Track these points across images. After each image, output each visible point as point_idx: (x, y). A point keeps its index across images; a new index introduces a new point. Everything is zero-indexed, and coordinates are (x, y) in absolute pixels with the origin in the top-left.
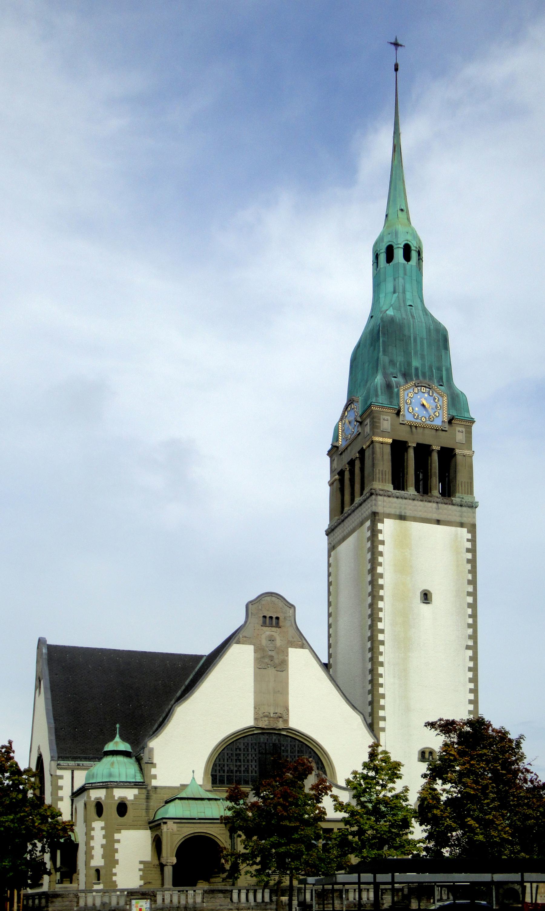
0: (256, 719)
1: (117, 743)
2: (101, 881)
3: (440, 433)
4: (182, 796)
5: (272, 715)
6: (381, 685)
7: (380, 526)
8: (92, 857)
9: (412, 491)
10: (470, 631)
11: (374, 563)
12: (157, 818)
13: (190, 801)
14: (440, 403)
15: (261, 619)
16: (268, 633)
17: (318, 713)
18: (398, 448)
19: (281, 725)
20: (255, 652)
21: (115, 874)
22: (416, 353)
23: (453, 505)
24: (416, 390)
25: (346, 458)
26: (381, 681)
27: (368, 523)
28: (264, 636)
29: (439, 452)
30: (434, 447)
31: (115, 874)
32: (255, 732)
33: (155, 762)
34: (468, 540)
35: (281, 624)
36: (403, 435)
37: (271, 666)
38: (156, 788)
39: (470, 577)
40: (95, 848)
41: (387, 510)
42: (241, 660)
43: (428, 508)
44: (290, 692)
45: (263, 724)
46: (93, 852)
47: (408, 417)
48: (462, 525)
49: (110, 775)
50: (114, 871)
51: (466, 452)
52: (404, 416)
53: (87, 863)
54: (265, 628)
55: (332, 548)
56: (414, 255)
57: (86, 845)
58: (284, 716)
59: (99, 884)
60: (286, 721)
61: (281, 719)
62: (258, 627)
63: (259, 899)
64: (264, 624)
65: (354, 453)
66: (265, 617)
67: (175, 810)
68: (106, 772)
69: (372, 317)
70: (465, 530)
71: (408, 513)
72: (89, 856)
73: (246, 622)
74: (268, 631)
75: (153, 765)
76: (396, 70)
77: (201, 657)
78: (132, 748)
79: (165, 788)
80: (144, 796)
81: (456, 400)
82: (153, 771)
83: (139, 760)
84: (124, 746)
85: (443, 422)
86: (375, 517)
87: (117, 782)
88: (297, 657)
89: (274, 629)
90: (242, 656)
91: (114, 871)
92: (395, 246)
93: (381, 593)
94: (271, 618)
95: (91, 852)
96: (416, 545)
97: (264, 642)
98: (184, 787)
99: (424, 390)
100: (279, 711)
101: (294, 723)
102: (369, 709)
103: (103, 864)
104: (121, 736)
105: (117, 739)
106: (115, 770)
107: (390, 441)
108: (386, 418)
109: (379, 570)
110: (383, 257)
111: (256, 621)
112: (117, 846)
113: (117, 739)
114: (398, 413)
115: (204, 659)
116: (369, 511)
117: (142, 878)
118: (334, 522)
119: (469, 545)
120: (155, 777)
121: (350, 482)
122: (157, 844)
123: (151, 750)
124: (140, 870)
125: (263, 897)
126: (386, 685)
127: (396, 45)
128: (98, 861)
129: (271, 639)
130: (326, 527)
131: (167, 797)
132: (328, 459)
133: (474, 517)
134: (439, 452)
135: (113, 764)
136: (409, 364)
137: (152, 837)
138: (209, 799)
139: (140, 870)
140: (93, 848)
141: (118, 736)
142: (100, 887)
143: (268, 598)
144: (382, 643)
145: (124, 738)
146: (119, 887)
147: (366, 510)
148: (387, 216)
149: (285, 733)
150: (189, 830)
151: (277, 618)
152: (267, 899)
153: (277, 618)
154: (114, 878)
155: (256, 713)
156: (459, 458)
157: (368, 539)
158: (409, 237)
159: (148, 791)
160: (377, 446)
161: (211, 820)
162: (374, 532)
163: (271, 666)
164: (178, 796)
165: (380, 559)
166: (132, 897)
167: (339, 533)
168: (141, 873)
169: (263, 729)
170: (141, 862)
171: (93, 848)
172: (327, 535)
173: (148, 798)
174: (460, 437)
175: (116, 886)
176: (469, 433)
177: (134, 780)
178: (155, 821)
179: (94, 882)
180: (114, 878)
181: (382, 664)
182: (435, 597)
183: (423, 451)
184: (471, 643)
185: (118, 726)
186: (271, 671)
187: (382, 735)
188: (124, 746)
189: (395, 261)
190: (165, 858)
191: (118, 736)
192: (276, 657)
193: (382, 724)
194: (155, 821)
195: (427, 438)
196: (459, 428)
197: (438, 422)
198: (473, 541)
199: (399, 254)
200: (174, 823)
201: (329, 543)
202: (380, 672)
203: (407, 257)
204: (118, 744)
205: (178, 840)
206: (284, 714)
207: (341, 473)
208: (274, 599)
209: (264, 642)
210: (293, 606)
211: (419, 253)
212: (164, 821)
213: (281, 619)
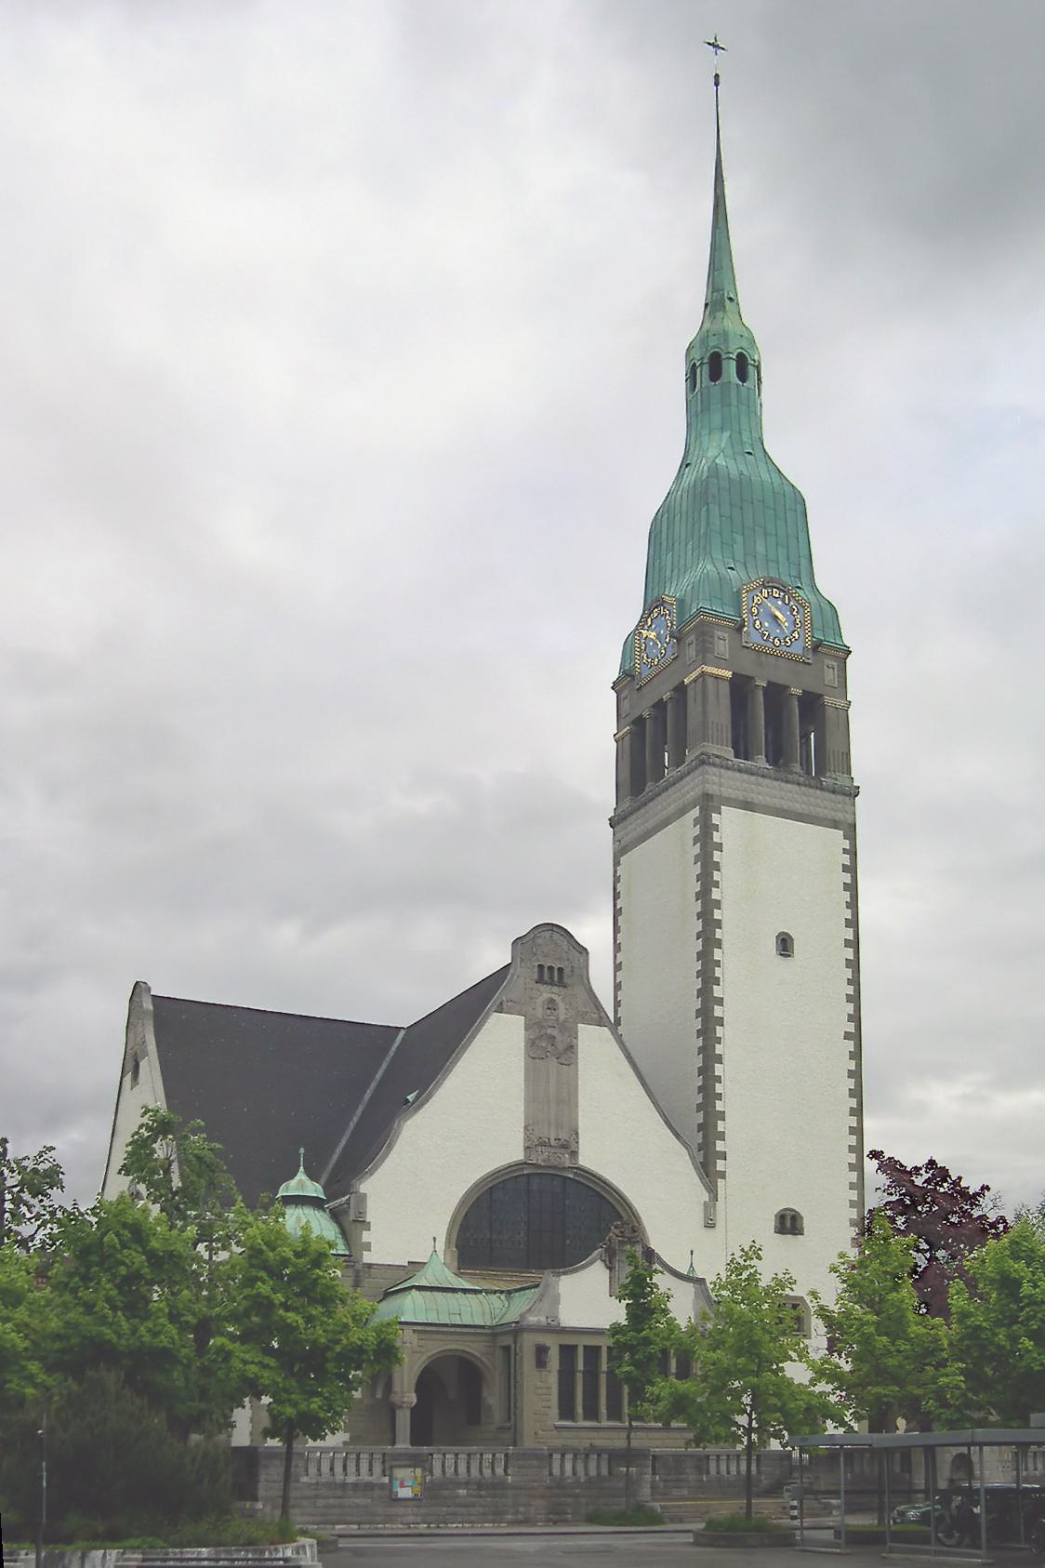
0: (527, 1148)
4: (424, 1283)
6: (719, 1097)
7: (715, 818)
9: (761, 762)
11: (707, 881)
16: (546, 996)
17: (621, 1141)
18: (740, 686)
19: (566, 1160)
23: (822, 789)
25: (650, 698)
26: (719, 1088)
27: (696, 812)
28: (540, 1001)
30: (793, 690)
34: (845, 851)
37: (551, 1051)
38: (370, 1266)
41: (726, 792)
42: (500, 1043)
43: (771, 790)
44: (581, 1102)
45: (539, 1158)
47: (755, 639)
48: (835, 824)
52: (748, 633)
54: (542, 987)
55: (620, 852)
56: (752, 371)
58: (569, 1146)
60: (574, 1154)
63: (593, 1473)
64: (540, 981)
66: (541, 967)
67: (413, 1307)
71: (758, 799)
74: (546, 993)
75: (367, 1226)
76: (717, 84)
81: (829, 615)
82: (366, 1237)
84: (314, 1190)
86: (708, 804)
88: (593, 1043)
89: (555, 989)
94: (551, 968)
96: (765, 852)
97: (540, 1013)
98: (416, 1266)
99: (776, 593)
100: (564, 1136)
101: (588, 1159)
102: (699, 1138)
105: (301, 1175)
107: (729, 674)
109: (716, 894)
110: (703, 374)
111: (526, 974)
113: (301, 1176)
116: (698, 791)
118: (626, 805)
119: (846, 859)
121: (655, 741)
125: (598, 1467)
126: (728, 1097)
129: (551, 1005)
131: (384, 1284)
138: (465, 1291)
143: (548, 934)
145: (313, 1176)
147: (691, 788)
150: (435, 1347)
151: (560, 970)
152: (605, 1471)
153: (560, 970)
155: (527, 1138)
156: (830, 711)
157: (696, 840)
158: (745, 345)
159: (357, 1272)
160: (710, 681)
163: (551, 1051)
165: (716, 876)
167: (635, 825)
169: (539, 1166)
174: (831, 676)
182: (772, 944)
183: (775, 693)
185: (302, 1150)
187: (720, 1182)
188: (314, 1190)
189: (724, 379)
192: (559, 1038)
193: (720, 1165)
197: (797, 649)
198: (852, 852)
199: (730, 369)
201: (616, 840)
203: (742, 375)
204: (301, 1184)
207: (639, 722)
208: (556, 936)
211: (758, 368)
213: (567, 971)
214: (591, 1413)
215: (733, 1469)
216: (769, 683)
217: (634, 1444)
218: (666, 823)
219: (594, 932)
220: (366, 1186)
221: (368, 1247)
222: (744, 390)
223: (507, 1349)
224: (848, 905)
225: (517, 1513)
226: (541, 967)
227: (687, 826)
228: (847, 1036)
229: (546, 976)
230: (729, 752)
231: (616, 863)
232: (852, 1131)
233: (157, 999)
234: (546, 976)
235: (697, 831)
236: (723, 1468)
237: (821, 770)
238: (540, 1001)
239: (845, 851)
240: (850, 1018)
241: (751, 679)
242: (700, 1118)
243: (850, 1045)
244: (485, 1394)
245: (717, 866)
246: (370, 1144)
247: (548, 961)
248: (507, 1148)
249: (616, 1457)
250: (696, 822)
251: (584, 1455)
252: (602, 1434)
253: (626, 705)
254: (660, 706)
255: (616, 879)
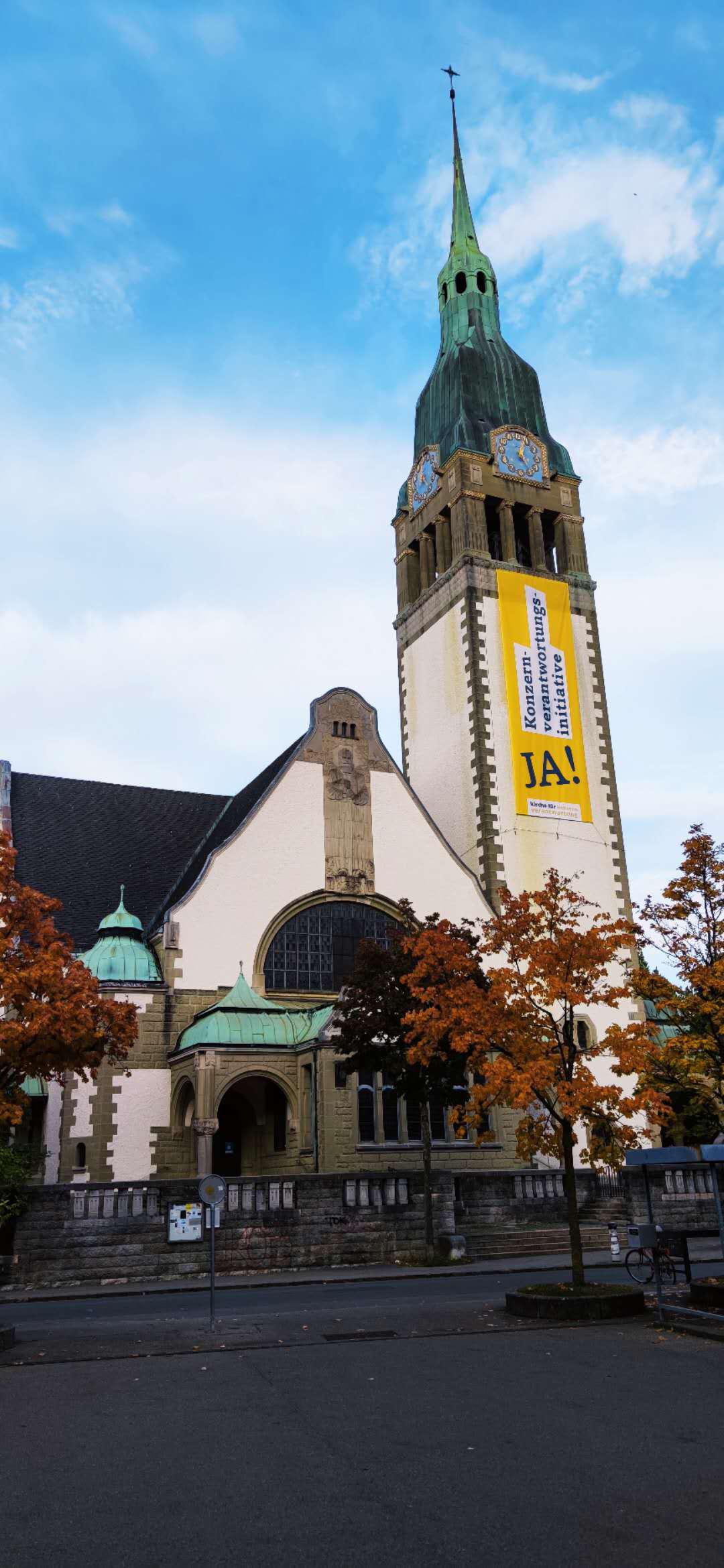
0: (329, 879)
1: (120, 915)
2: (86, 1167)
3: (542, 491)
4: (229, 1004)
5: (351, 874)
7: (478, 606)
8: (73, 1121)
9: (513, 562)
10: (604, 758)
12: (183, 1045)
13: (241, 1015)
14: (539, 455)
15: (332, 726)
16: (341, 747)
19: (363, 889)
20: (325, 773)
21: (111, 1154)
22: (503, 395)
24: (509, 436)
25: (421, 524)
27: (462, 603)
28: (336, 751)
29: (541, 515)
31: (111, 1154)
32: (328, 900)
33: (180, 947)
34: (588, 632)
35: (358, 734)
36: (498, 490)
37: (348, 789)
38: (181, 992)
39: (595, 681)
40: (79, 1103)
45: (340, 886)
46: (77, 1112)
47: (504, 469)
49: (111, 970)
50: (110, 1146)
51: (575, 518)
53: (63, 1132)
54: (337, 740)
55: (404, 644)
56: (489, 284)
57: (63, 1098)
58: (364, 877)
59: (83, 1172)
60: (371, 883)
61: (363, 881)
62: (329, 737)
64: (335, 735)
65: (432, 516)
66: (336, 723)
67: (217, 1029)
68: (104, 964)
69: (443, 354)
70: (583, 618)
72: (67, 1118)
73: (312, 729)
74: (341, 744)
77: (227, 798)
78: (143, 924)
79: (193, 992)
80: (161, 1007)
81: (557, 455)
82: (178, 963)
83: (151, 947)
85: (544, 478)
86: (472, 594)
87: (120, 982)
89: (349, 741)
90: (306, 779)
91: (110, 1146)
92: (467, 274)
93: (487, 697)
95: (72, 1111)
97: (337, 760)
98: (225, 989)
101: (379, 889)
103: (91, 1134)
104: (126, 907)
105: (121, 909)
106: (118, 960)
107: (483, 496)
108: (477, 467)
110: (452, 288)
112: (116, 1098)
113: (121, 909)
114: (491, 462)
115: (229, 803)
117: (154, 1160)
119: (590, 639)
120: (180, 973)
122: (184, 1094)
123: (175, 928)
124: (152, 1144)
127: (451, 72)
128: (82, 1129)
129: (347, 755)
130: (394, 619)
132: (392, 530)
133: (593, 602)
134: (541, 515)
135: (114, 949)
136: (496, 407)
137: (172, 1082)
139: (152, 1144)
140: (75, 1103)
141: (121, 904)
142: (84, 1178)
144: (493, 769)
145: (130, 909)
146: (116, 1179)
147: (460, 581)
148: (452, 244)
149: (368, 903)
150: (241, 1066)
151: (353, 726)
152: (404, 1200)
153: (353, 726)
154: (109, 1161)
155: (328, 869)
156: (568, 525)
159: (168, 998)
161: (277, 1048)
162: (472, 615)
163: (348, 789)
164: (220, 1005)
166: (171, 1199)
167: (414, 623)
168: (153, 1151)
169: (339, 895)
170: (154, 1130)
171: (75, 1103)
172: (396, 628)
173: (168, 1010)
174: (566, 498)
175: (112, 1176)
176: (575, 494)
177: (146, 979)
178: (182, 1052)
179: (74, 1168)
180: (109, 1161)
181: (491, 752)
183: (521, 510)
184: (606, 775)
185: (122, 887)
186: (347, 804)
190: (201, 1120)
191: (121, 904)
194: (182, 1052)
195: (525, 496)
196: (562, 488)
197: (537, 478)
198: (594, 632)
199: (472, 283)
200: (217, 1053)
201: (400, 639)
202: (493, 812)
204: (121, 918)
205: (223, 1083)
206: (368, 874)
208: (348, 697)
209: (337, 760)
210: (373, 709)
212: (202, 1049)
214: (391, 1133)
215: (540, 1191)
216: (517, 503)
217: (434, 1165)
218: (439, 616)
219: (380, 693)
220: (180, 916)
221: (180, 973)
222: (484, 298)
223: (308, 1067)
224: (595, 675)
225: (308, 1253)
226: (336, 723)
227: (458, 614)
228: (604, 781)
229: (340, 732)
230: (488, 557)
231: (400, 655)
232: (619, 894)
233: (14, 775)
234: (340, 732)
235: (464, 616)
236: (529, 1190)
237: (564, 568)
238: (336, 751)
239: (588, 632)
240: (605, 766)
241: (500, 500)
242: (480, 851)
243: (607, 789)
244: (289, 1116)
245: (482, 643)
246: (183, 883)
247: (341, 722)
248: (310, 878)
249: (418, 1181)
250: (463, 610)
251: (378, 1180)
252: (404, 1155)
253: (403, 535)
254: (430, 529)
255: (401, 668)
